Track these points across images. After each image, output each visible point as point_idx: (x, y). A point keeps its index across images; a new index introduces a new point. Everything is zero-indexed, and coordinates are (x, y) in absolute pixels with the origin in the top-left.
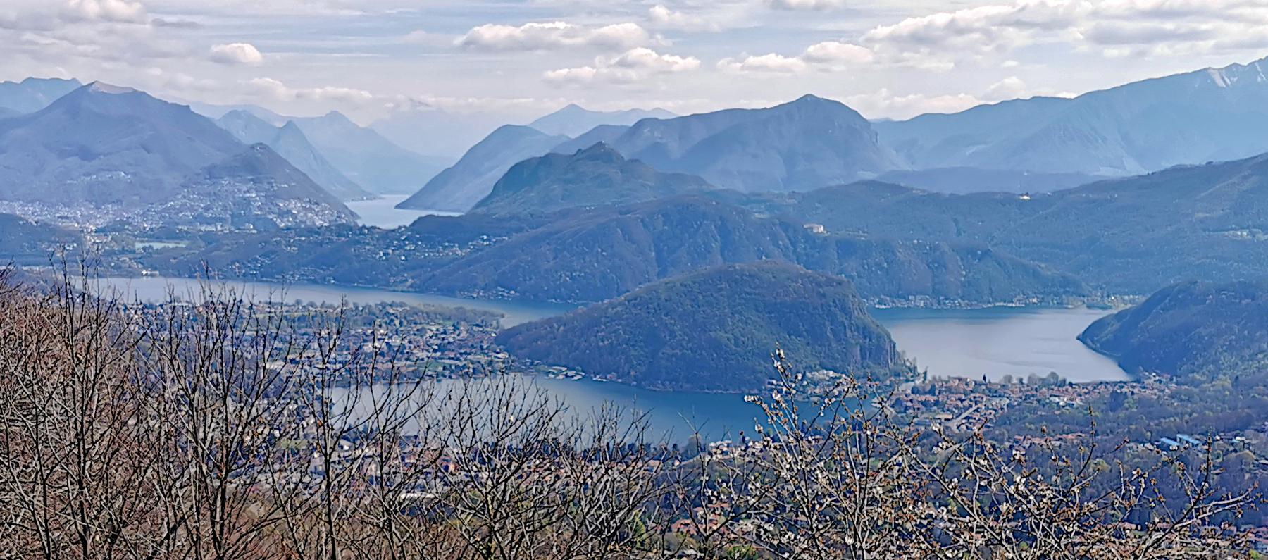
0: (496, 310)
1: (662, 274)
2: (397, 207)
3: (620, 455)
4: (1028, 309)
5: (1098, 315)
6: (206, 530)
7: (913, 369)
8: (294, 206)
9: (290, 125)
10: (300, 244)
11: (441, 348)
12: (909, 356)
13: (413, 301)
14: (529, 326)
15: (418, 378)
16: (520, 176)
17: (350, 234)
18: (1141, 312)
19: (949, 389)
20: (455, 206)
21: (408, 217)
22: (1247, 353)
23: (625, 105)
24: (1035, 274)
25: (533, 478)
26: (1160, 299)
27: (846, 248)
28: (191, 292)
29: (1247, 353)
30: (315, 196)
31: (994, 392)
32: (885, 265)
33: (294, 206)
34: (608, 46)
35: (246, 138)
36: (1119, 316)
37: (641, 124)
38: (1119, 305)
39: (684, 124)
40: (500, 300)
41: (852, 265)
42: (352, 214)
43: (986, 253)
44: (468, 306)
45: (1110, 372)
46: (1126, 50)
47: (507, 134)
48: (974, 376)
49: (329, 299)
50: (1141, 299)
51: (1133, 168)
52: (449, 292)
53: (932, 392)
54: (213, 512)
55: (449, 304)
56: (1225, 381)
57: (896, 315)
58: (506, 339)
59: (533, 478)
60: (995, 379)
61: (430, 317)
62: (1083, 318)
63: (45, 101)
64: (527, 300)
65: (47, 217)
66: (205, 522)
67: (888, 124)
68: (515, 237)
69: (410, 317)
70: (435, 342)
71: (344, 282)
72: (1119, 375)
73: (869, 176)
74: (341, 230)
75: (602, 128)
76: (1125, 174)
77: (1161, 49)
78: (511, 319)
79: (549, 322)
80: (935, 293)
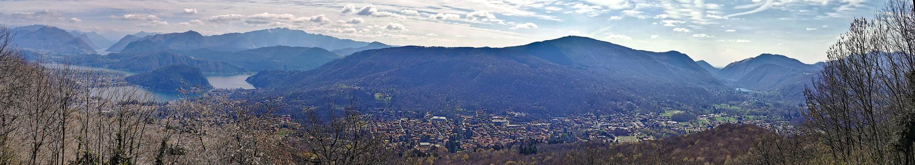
0: (125, 73)
1: (160, 66)
2: (106, 51)
3: (151, 104)
4: (235, 75)
5: (249, 76)
6: (62, 112)
7: (212, 87)
8: (84, 50)
9: (84, 34)
10: (85, 58)
11: (113, 80)
12: (211, 84)
13: (108, 70)
14: (132, 76)
15: (108, 86)
16: (132, 45)
17: (96, 56)
18: (258, 75)
19: (220, 91)
20: (117, 51)
21: (107, 53)
22: (277, 83)
23: (153, 31)
24: (237, 68)
25: (132, 107)
26: (261, 73)
27: (198, 62)
28: (62, 67)
29: (277, 83)
30: (89, 48)
31: (229, 92)
32: (823, 132)
33: (84, 50)
34: (149, 20)
35: (75, 36)
36: (253, 76)
37: (156, 36)
38: (253, 74)
39: (165, 36)
40: (125, 70)
41: (200, 65)
42: (96, 52)
43: (227, 63)
44: (119, 72)
45: (251, 87)
46: (253, 25)
47: (128, 37)
48: (224, 88)
49: (90, 69)
50: (257, 73)
51: (255, 47)
52: (115, 68)
53: (216, 92)
54: (63, 108)
55: (115, 71)
56: (273, 89)
57: (209, 75)
58: (127, 79)
59: (132, 107)
60: (229, 89)
61: (111, 74)
62: (247, 77)
63: (37, 29)
64: (132, 70)
65: (36, 51)
66: (62, 110)
67: (207, 37)
68: (129, 58)
69: (106, 74)
70: (112, 79)
71: (93, 66)
72: (254, 88)
73: (203, 47)
74: (94, 55)
75: (148, 36)
76: (253, 48)
77: (259, 25)
78: (128, 75)
79: (136, 75)
80: (217, 71)
